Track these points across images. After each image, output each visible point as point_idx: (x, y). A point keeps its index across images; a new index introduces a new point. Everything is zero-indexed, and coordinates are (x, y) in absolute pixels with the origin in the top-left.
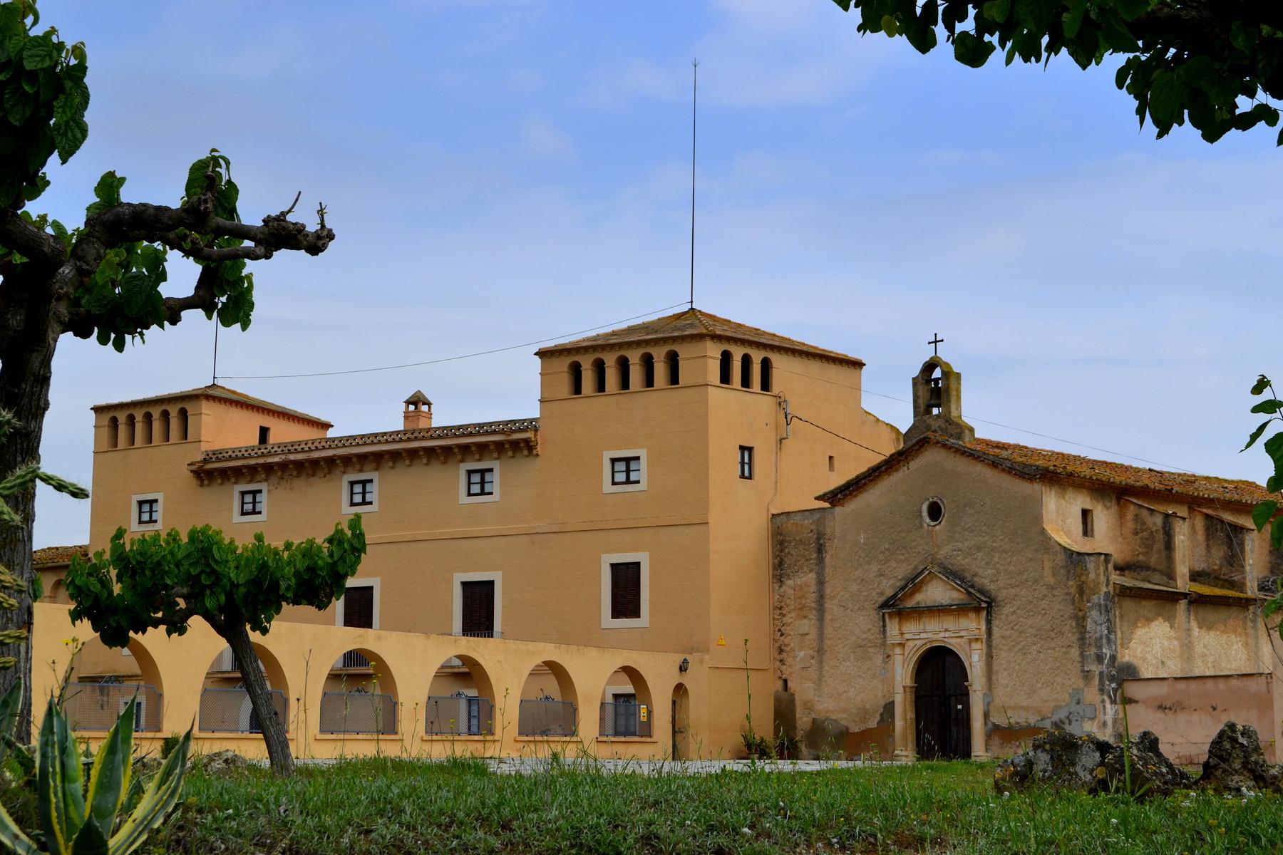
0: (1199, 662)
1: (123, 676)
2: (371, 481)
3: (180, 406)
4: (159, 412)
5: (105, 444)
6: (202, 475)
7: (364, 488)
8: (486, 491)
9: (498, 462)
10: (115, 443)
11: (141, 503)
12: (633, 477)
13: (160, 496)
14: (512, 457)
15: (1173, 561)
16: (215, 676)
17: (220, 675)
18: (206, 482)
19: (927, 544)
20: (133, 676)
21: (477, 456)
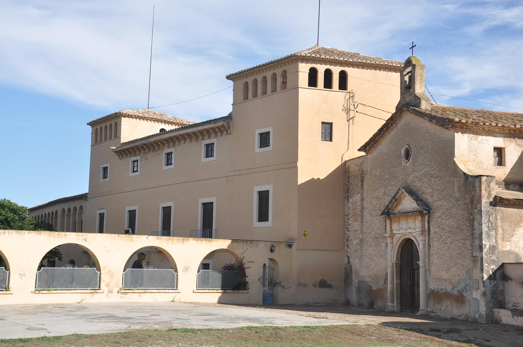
5: (241, 97)
10: (246, 98)
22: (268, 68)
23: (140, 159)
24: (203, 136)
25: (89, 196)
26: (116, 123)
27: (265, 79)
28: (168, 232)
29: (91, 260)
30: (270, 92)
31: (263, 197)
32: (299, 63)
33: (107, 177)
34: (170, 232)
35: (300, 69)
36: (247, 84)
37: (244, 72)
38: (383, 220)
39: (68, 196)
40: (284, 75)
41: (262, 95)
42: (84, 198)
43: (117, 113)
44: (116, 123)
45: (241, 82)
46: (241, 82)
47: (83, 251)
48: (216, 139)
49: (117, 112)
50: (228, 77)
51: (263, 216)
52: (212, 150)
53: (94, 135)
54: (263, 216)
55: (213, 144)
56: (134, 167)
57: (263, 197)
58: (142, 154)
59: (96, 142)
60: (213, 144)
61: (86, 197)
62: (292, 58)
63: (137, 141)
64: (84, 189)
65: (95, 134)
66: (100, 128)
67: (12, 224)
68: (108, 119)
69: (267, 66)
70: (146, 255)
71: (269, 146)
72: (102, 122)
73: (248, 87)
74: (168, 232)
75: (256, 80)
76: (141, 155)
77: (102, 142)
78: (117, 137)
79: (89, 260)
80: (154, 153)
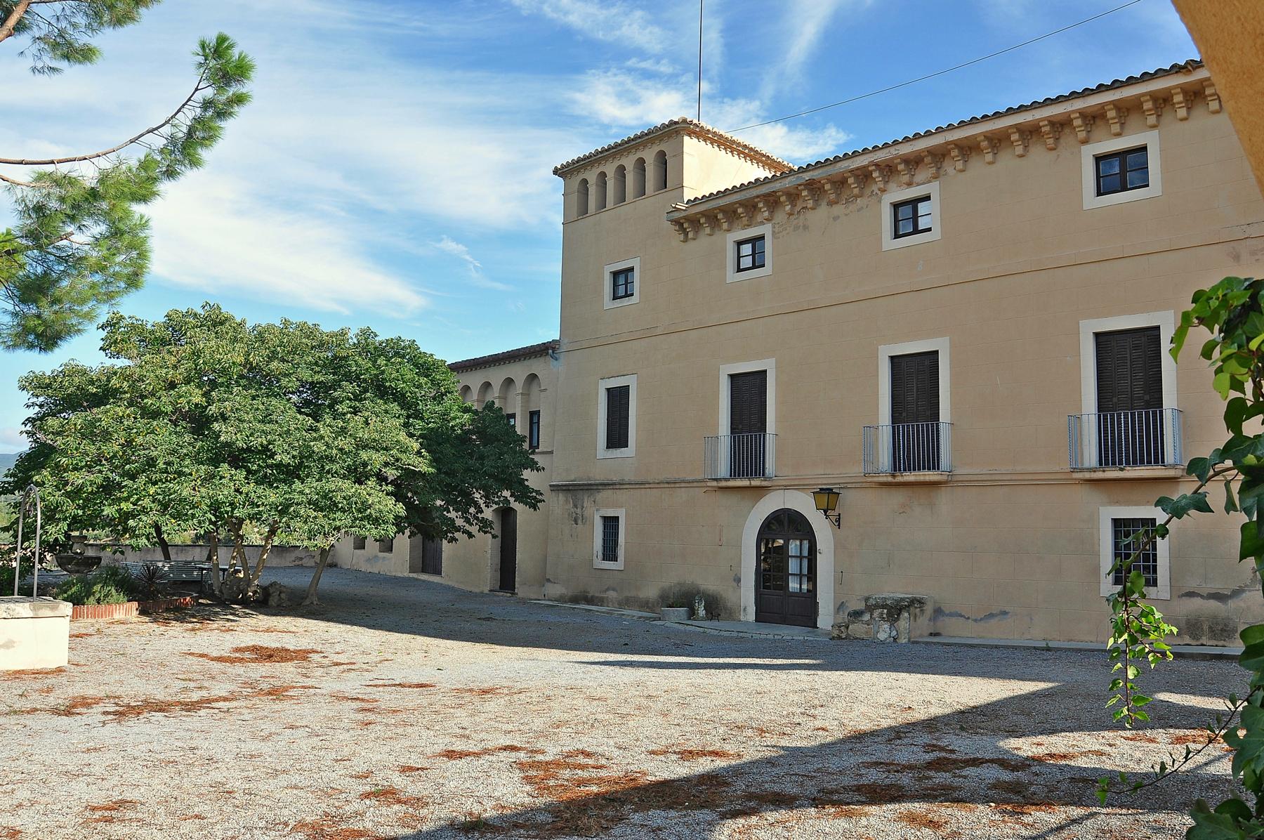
0: (1228, 772)
1: (597, 485)
2: (927, 198)
3: (656, 149)
4: (595, 177)
5: (574, 210)
6: (686, 225)
7: (915, 211)
8: (920, 228)
9: (1155, 132)
10: (584, 210)
11: (616, 275)
12: (922, 224)
13: (635, 263)
14: (728, 230)
15: (1254, 487)
16: (709, 484)
17: (715, 484)
18: (691, 235)
19: (294, 511)
20: (609, 484)
21: (1116, 128)
22: (657, 138)
23: (773, 232)
24: (772, 210)
25: (564, 348)
30: (652, 190)
31: (618, 398)
32: (686, 139)
36: (585, 182)
37: (613, 148)
39: (487, 355)
40: (662, 159)
43: (676, 123)
47: (550, 486)
49: (677, 120)
50: (556, 172)
51: (617, 437)
54: (617, 437)
57: (618, 398)
59: (584, 210)
61: (554, 349)
64: (550, 332)
67: (421, 407)
68: (639, 144)
69: (650, 137)
70: (839, 494)
71: (763, 266)
72: (606, 159)
75: (603, 175)
78: (666, 187)
79: (575, 506)
80: (838, 209)
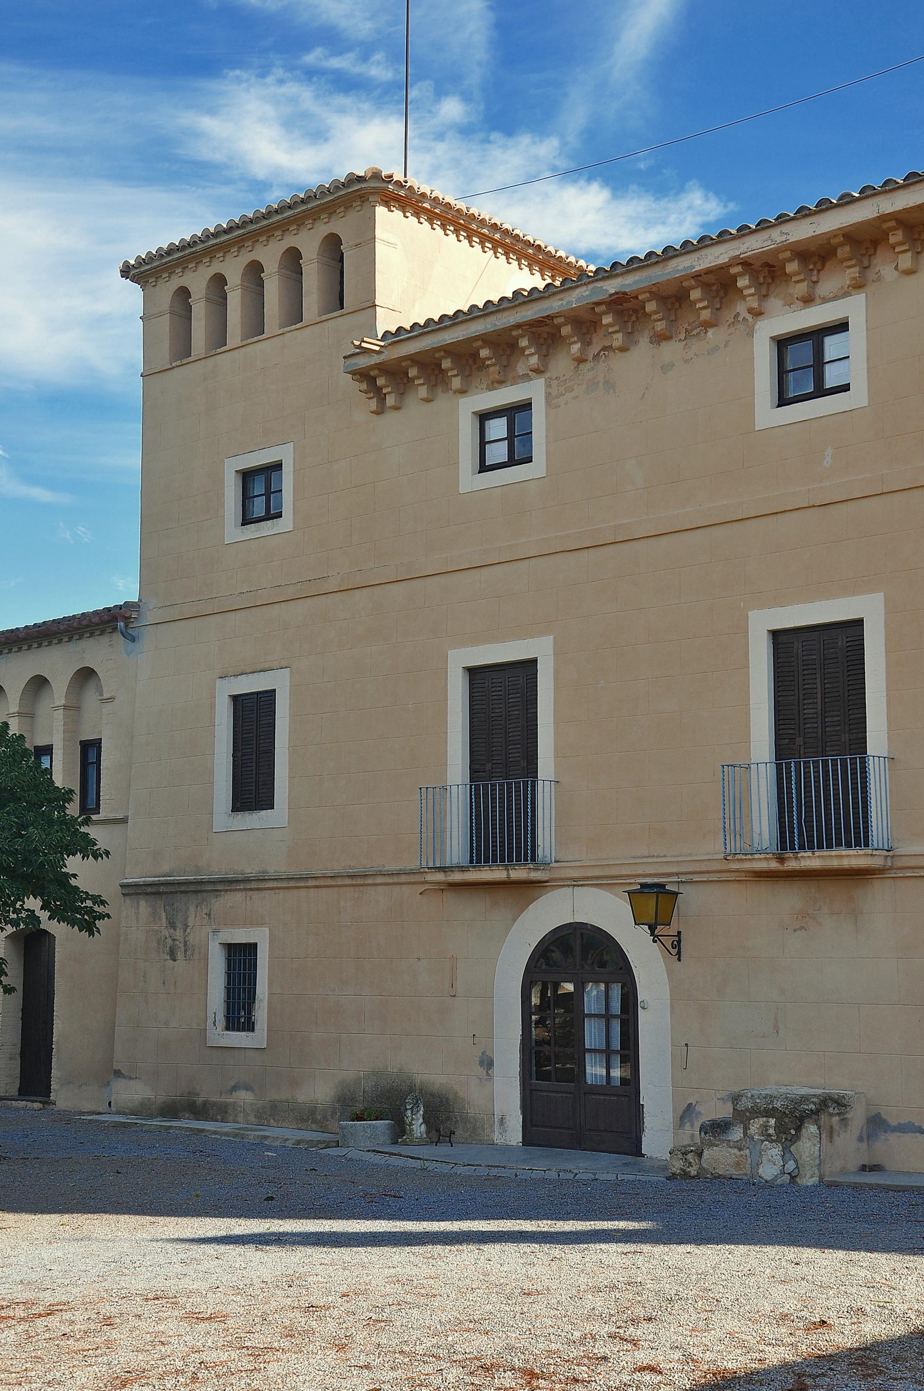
23: (548, 396)
25: (149, 617)
26: (333, 244)
27: (255, 270)
28: (853, 763)
29: (186, 926)
33: (279, 515)
34: (863, 762)
35: (380, 232)
36: (184, 293)
38: (254, 872)
41: (246, 336)
42: (121, 624)
43: (360, 179)
44: (333, 244)
45: (166, 290)
46: (166, 290)
48: (862, 296)
49: (362, 174)
52: (272, 492)
53: (165, 323)
55: (277, 466)
56: (483, 443)
58: (561, 364)
60: (277, 466)
62: (309, 206)
63: (473, 313)
65: (167, 317)
66: (204, 284)
70: (677, 894)
72: (224, 248)
73: (189, 309)
74: (853, 763)
75: (219, 281)
76: (548, 375)
77: (191, 359)
79: (172, 925)
